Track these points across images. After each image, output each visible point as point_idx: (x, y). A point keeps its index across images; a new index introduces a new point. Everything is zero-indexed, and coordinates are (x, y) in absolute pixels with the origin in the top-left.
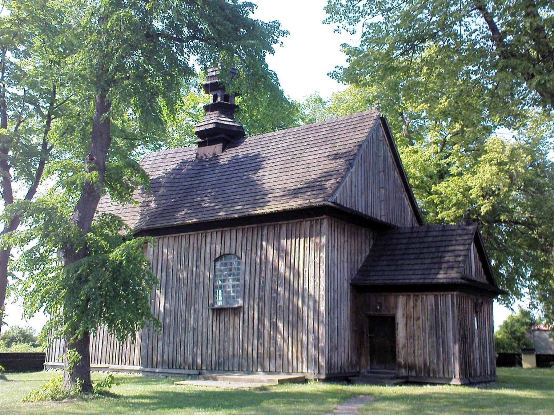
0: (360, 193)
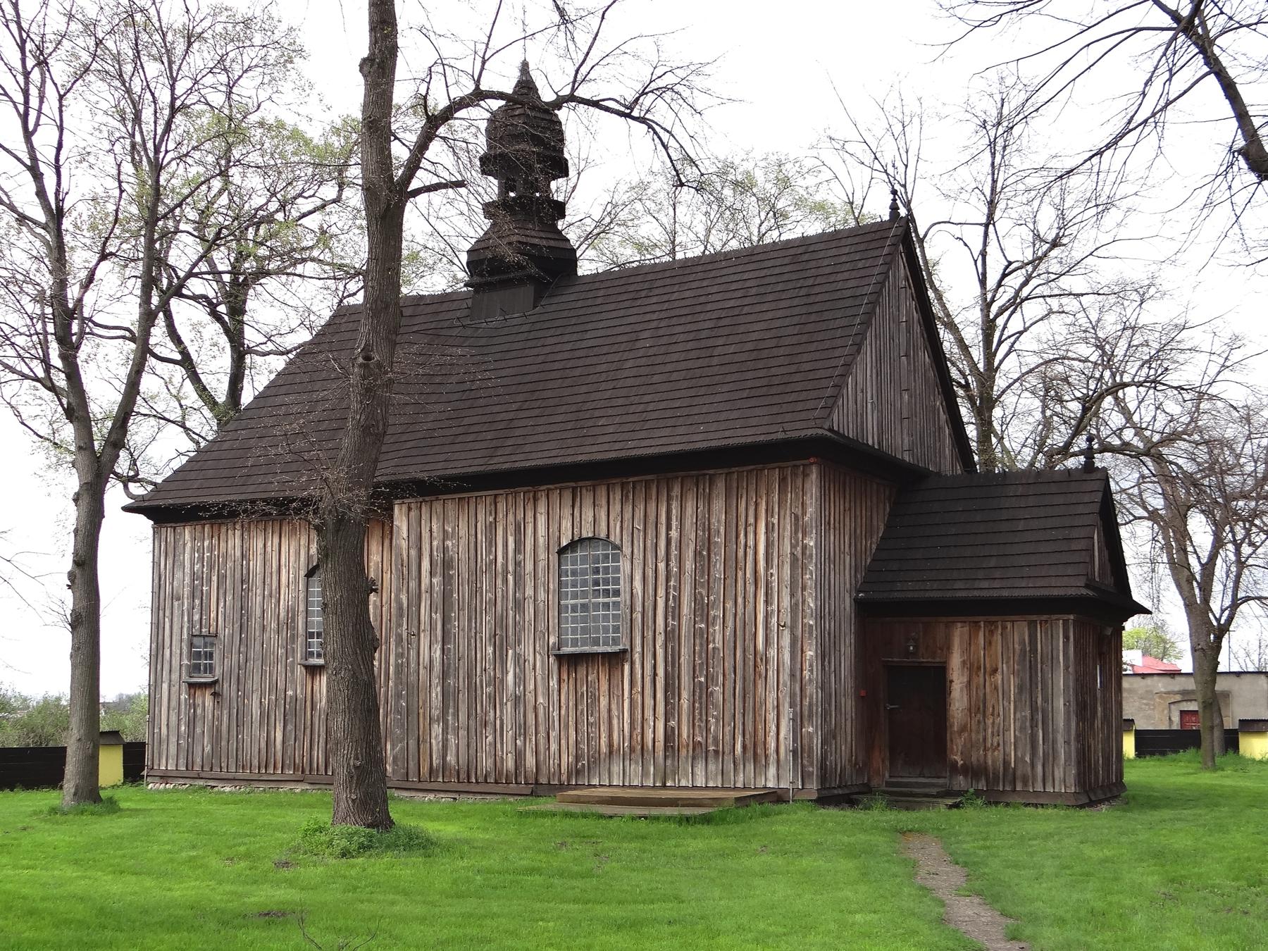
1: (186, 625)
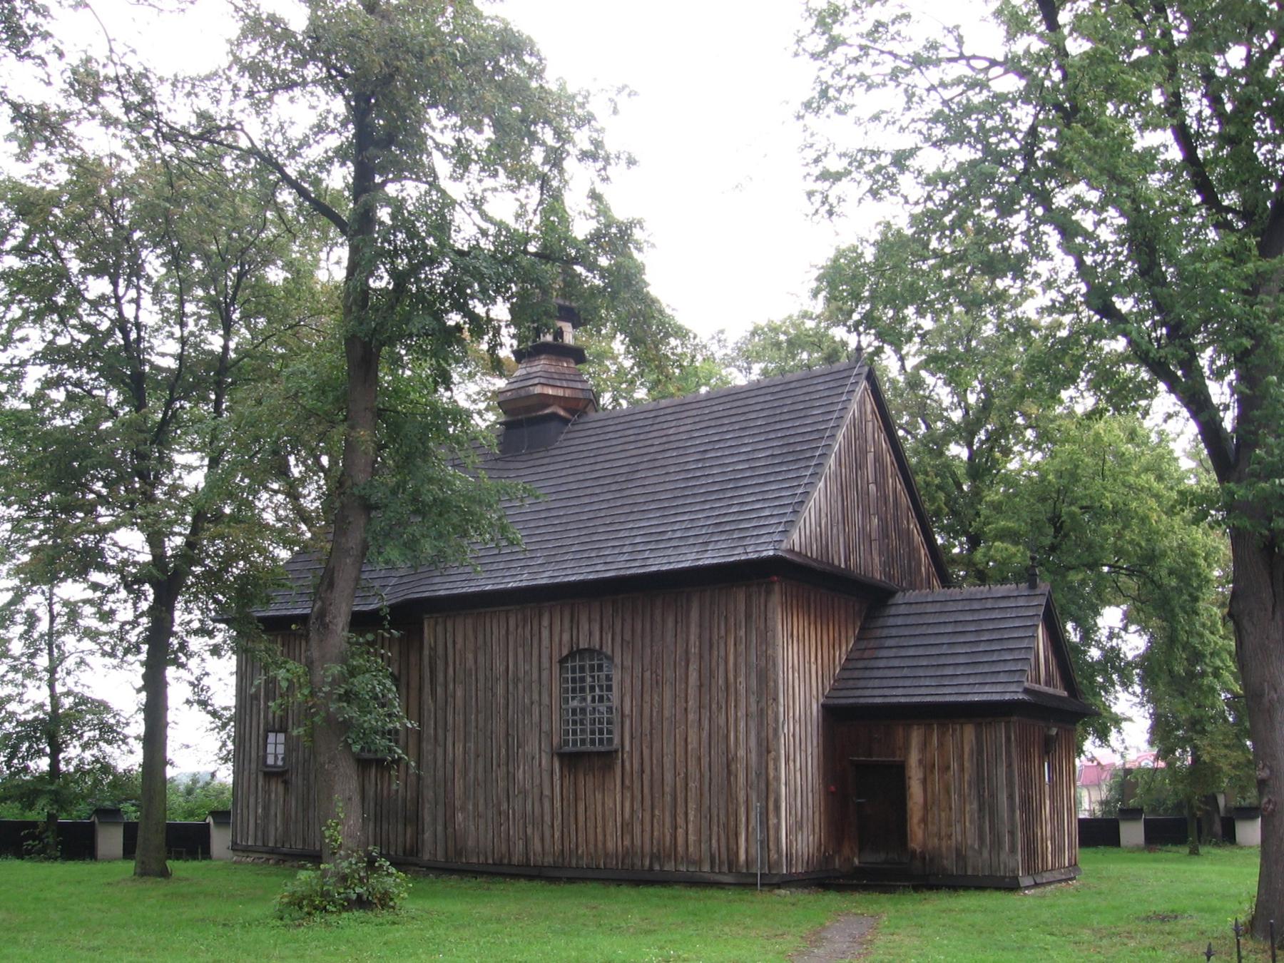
1: (262, 721)
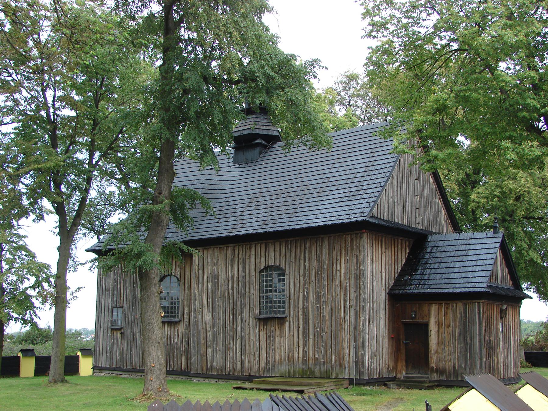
0: (396, 204)
1: (111, 302)
